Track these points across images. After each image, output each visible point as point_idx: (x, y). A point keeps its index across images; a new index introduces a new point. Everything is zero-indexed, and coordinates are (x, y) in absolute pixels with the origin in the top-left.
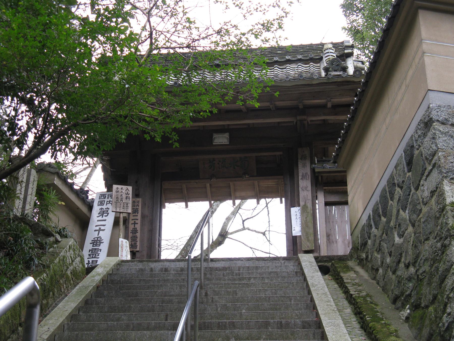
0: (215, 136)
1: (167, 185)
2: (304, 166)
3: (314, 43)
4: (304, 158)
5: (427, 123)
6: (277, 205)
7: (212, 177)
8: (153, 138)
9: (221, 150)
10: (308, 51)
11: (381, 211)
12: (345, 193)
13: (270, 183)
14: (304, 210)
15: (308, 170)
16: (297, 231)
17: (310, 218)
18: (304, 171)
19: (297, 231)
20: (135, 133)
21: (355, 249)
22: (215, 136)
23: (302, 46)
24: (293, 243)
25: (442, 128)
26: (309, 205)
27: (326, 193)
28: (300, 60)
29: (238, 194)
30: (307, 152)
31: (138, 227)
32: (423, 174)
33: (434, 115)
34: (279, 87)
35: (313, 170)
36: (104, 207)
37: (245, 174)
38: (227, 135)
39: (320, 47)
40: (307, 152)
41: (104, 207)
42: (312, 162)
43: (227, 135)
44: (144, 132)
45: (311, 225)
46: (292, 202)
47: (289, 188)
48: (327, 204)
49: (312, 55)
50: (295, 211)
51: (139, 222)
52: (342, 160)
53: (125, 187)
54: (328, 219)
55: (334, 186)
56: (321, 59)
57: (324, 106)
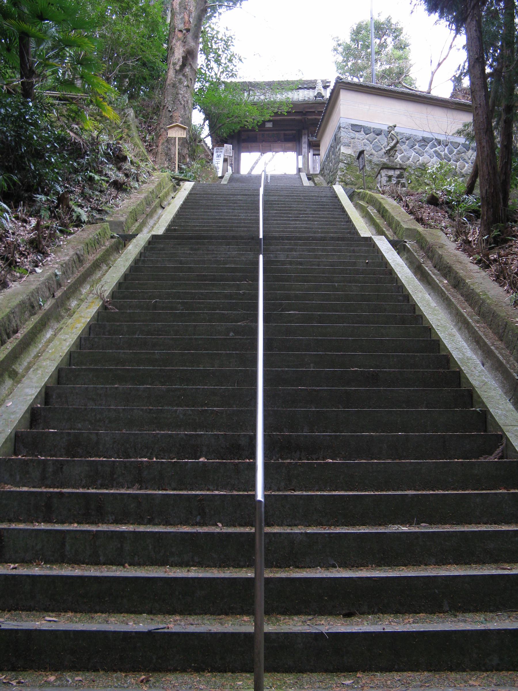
0: (266, 123)
1: (243, 145)
2: (305, 138)
3: (281, 153)
4: (305, 134)
5: (339, 128)
6: (292, 155)
7: (263, 141)
8: (248, 127)
9: (269, 130)
10: (309, 83)
11: (328, 156)
12: (319, 150)
13: (290, 145)
14: (304, 157)
15: (307, 140)
16: (300, 166)
17: (306, 160)
18: (304, 140)
19: (300, 166)
20: (243, 126)
21: (321, 171)
22: (266, 123)
23: (307, 81)
24: (299, 170)
25: (343, 129)
26: (306, 155)
27: (314, 150)
28: (305, 88)
29: (275, 150)
30: (306, 132)
31: (233, 162)
32: (338, 144)
33: (341, 125)
34: (295, 104)
35: (308, 140)
36: (219, 154)
37: (278, 140)
38: (271, 123)
39: (315, 82)
40: (306, 132)
41: (219, 154)
42: (308, 136)
43: (271, 123)
44: (245, 125)
45: (306, 163)
46: (299, 153)
47: (298, 148)
48: (314, 155)
49: (311, 85)
50: (300, 157)
51: (233, 160)
52: (319, 136)
53: (229, 145)
54: (314, 161)
55: (315, 146)
56: (315, 88)
57: (314, 112)
